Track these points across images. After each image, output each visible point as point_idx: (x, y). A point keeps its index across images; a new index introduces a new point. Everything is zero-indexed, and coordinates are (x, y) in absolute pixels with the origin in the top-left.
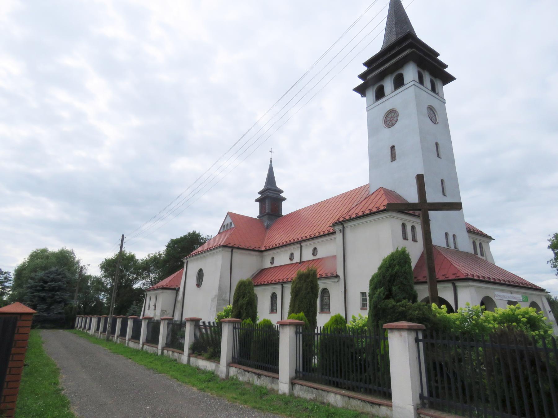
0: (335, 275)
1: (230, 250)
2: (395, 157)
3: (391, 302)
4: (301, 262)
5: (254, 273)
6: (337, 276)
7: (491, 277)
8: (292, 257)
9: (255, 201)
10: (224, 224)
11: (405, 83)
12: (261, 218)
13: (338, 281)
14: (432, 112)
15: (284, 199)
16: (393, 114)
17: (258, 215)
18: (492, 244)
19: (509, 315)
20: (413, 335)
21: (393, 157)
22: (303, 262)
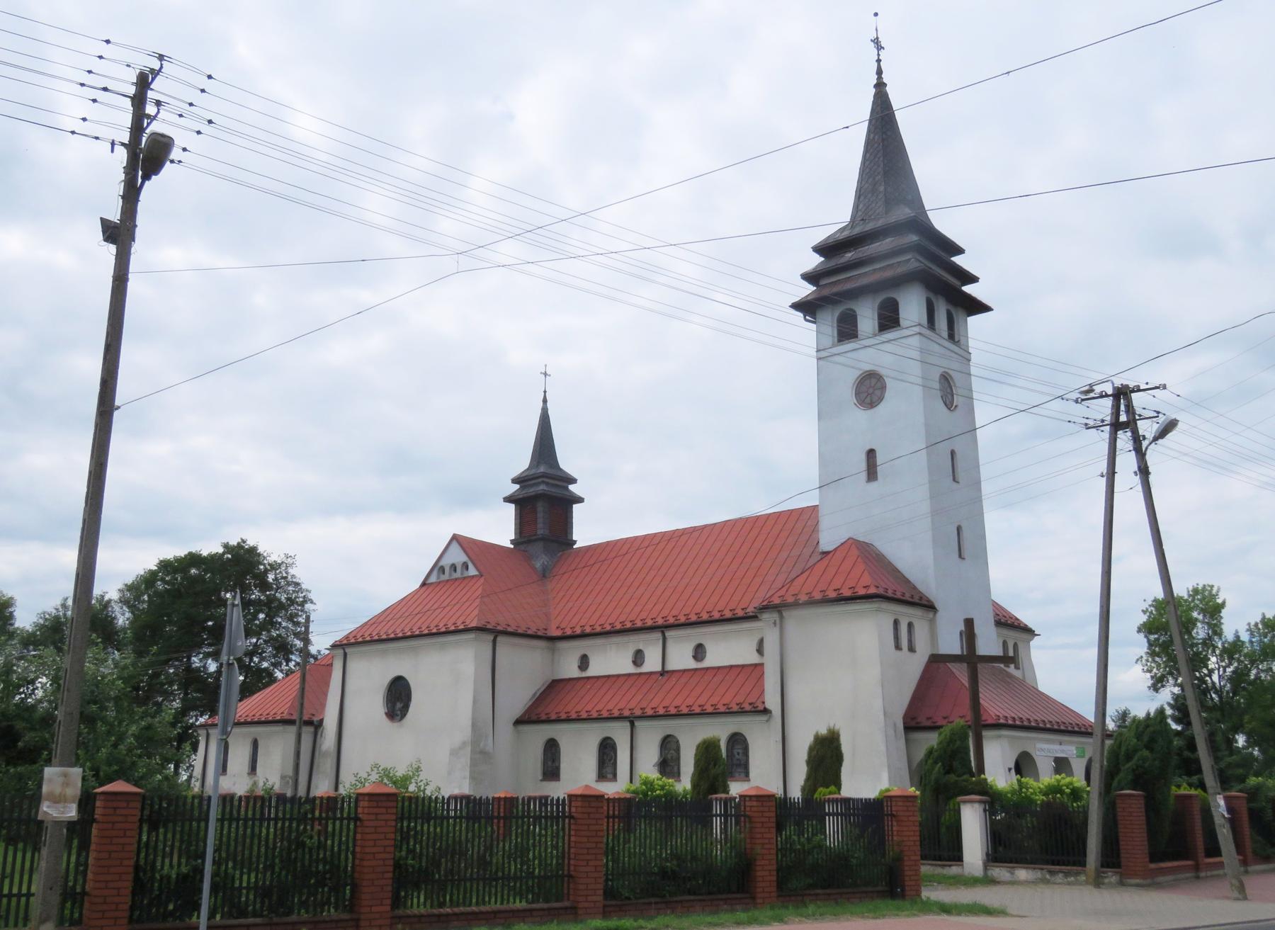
0: (761, 708)
1: (491, 637)
2: (876, 472)
3: (952, 778)
4: (663, 673)
5: (536, 689)
6: (766, 711)
7: (1033, 717)
8: (638, 658)
9: (504, 501)
10: (442, 563)
11: (902, 322)
12: (522, 547)
13: (767, 721)
14: (947, 385)
15: (580, 500)
16: (874, 381)
17: (513, 538)
18: (1035, 643)
19: (1054, 786)
20: (983, 806)
21: (872, 473)
22: (667, 672)
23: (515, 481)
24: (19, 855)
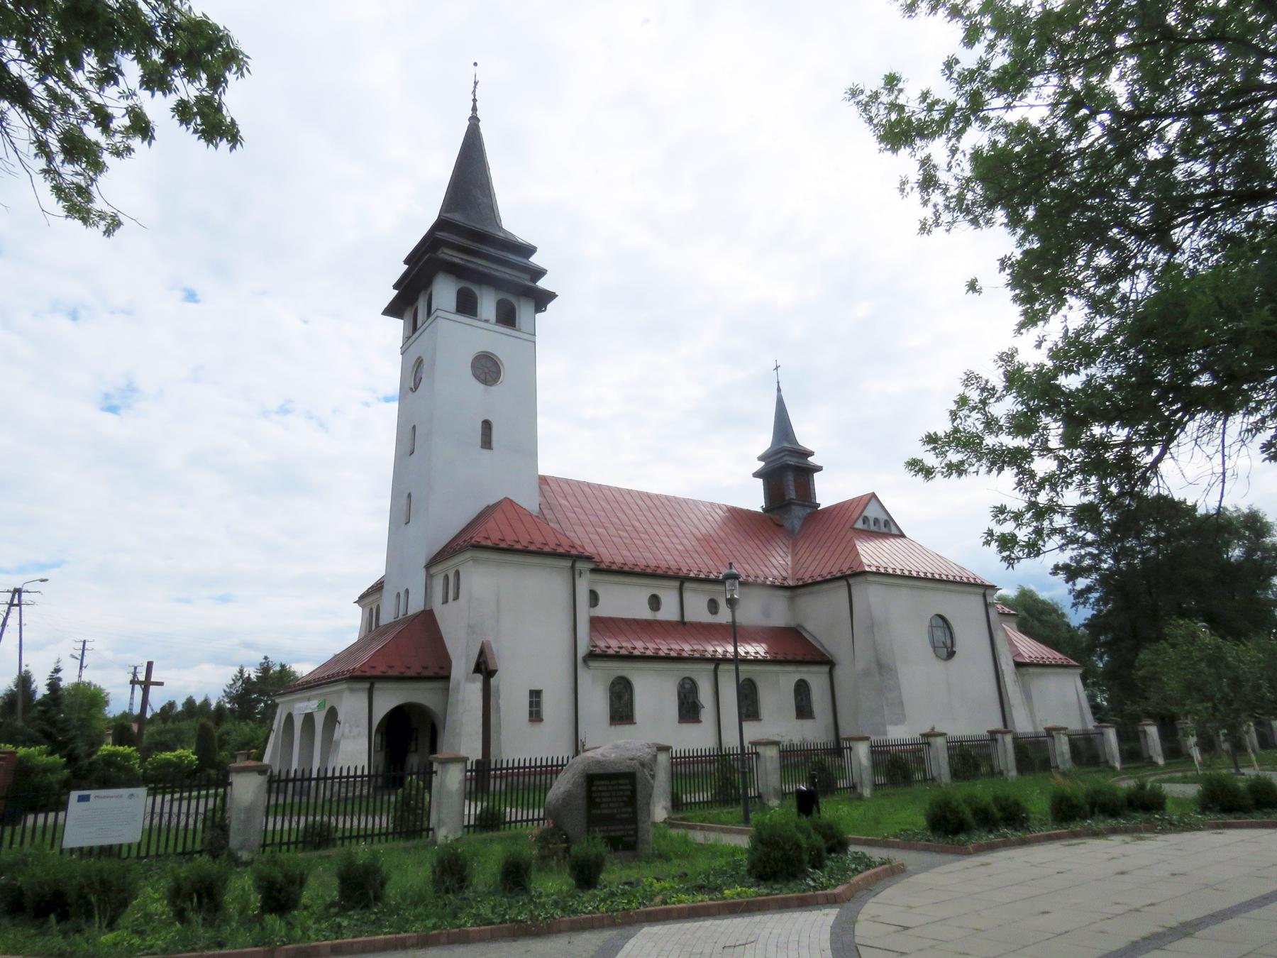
21: (487, 443)
23: (761, 458)
24: (531, 795)
